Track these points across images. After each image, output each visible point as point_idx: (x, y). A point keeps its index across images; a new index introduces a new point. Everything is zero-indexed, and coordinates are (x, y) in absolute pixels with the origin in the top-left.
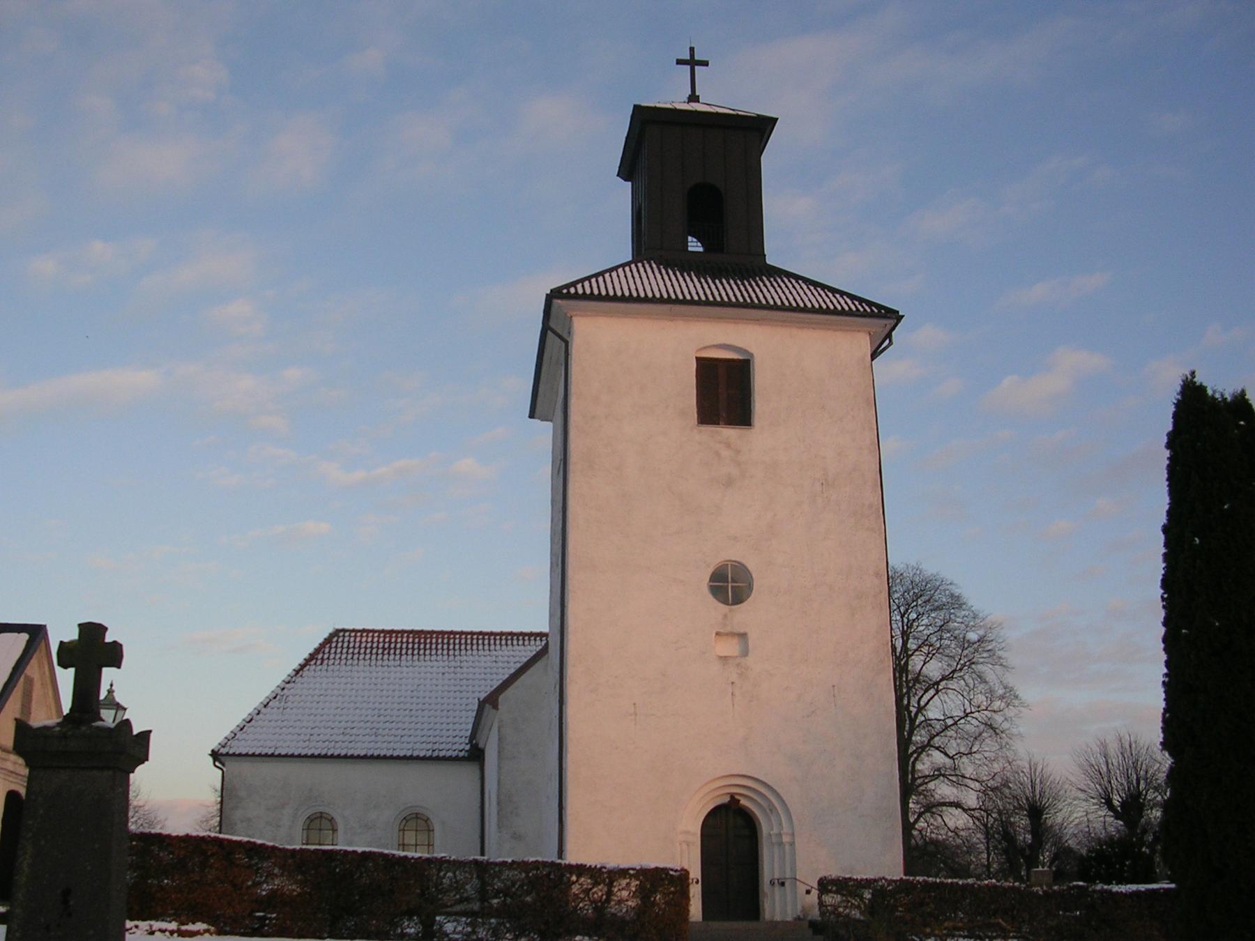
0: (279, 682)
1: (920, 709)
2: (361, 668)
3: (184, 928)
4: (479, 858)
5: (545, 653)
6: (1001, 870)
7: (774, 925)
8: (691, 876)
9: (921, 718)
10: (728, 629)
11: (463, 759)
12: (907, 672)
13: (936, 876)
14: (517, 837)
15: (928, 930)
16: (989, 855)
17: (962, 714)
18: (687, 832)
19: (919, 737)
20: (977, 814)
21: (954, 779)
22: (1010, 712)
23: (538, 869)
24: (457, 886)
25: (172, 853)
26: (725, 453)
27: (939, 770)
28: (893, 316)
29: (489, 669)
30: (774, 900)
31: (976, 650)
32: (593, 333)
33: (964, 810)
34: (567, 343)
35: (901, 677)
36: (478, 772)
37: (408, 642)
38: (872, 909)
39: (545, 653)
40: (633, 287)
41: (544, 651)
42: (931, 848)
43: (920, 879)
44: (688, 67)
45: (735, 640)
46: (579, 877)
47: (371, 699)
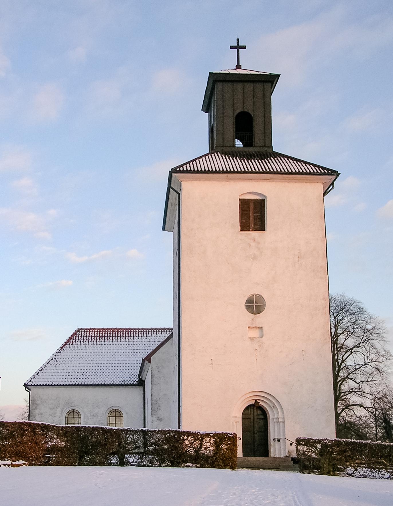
0: (53, 352)
1: (343, 361)
2: (90, 345)
3: (14, 463)
4: (144, 429)
5: (172, 337)
6: (383, 436)
7: (275, 459)
9: (343, 365)
10: (254, 325)
11: (136, 385)
12: (337, 343)
13: (351, 439)
14: (160, 419)
15: (348, 464)
16: (377, 429)
17: (364, 364)
18: (236, 417)
19: (343, 374)
20: (370, 410)
21: (359, 393)
22: (388, 362)
23: (170, 433)
24: (135, 442)
25: (8, 430)
26: (253, 244)
27: (352, 389)
28: (334, 173)
29: (144, 346)
30: (275, 447)
31: (371, 334)
32: (191, 189)
33: (364, 408)
34: (179, 194)
35: (334, 346)
36: (142, 389)
37: (110, 334)
38: (321, 453)
39: (172, 337)
40: (210, 166)
41: (171, 336)
42: (348, 425)
43: (344, 440)
44: (240, 45)
45: (258, 330)
46: (188, 437)
47: (95, 359)
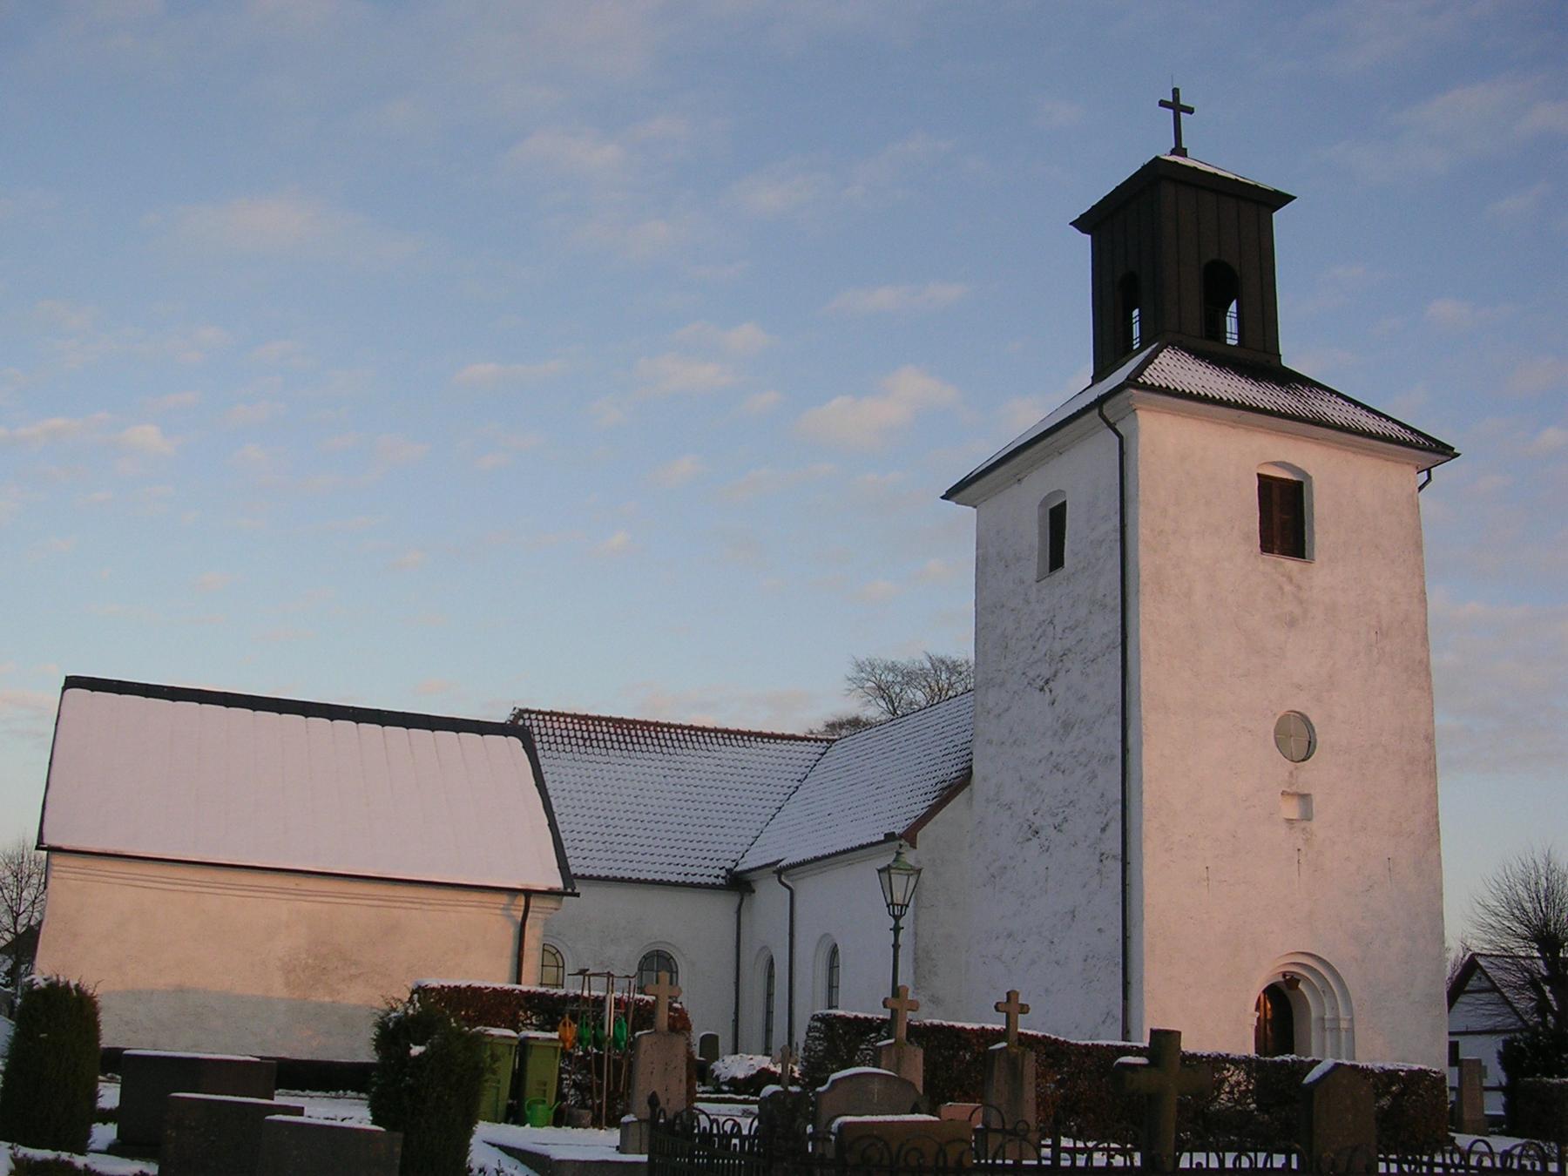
8: (1448, 1083)
10: (1294, 789)
26: (1288, 588)
28: (1445, 452)
45: (1295, 802)
